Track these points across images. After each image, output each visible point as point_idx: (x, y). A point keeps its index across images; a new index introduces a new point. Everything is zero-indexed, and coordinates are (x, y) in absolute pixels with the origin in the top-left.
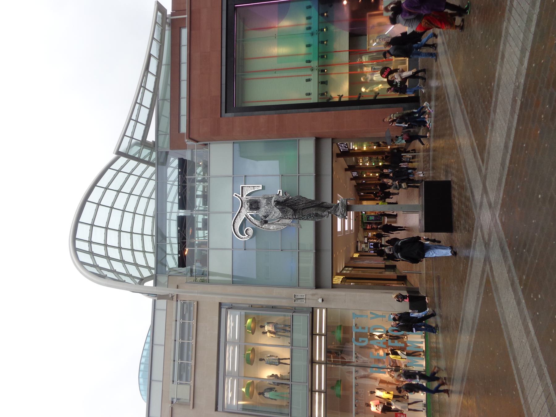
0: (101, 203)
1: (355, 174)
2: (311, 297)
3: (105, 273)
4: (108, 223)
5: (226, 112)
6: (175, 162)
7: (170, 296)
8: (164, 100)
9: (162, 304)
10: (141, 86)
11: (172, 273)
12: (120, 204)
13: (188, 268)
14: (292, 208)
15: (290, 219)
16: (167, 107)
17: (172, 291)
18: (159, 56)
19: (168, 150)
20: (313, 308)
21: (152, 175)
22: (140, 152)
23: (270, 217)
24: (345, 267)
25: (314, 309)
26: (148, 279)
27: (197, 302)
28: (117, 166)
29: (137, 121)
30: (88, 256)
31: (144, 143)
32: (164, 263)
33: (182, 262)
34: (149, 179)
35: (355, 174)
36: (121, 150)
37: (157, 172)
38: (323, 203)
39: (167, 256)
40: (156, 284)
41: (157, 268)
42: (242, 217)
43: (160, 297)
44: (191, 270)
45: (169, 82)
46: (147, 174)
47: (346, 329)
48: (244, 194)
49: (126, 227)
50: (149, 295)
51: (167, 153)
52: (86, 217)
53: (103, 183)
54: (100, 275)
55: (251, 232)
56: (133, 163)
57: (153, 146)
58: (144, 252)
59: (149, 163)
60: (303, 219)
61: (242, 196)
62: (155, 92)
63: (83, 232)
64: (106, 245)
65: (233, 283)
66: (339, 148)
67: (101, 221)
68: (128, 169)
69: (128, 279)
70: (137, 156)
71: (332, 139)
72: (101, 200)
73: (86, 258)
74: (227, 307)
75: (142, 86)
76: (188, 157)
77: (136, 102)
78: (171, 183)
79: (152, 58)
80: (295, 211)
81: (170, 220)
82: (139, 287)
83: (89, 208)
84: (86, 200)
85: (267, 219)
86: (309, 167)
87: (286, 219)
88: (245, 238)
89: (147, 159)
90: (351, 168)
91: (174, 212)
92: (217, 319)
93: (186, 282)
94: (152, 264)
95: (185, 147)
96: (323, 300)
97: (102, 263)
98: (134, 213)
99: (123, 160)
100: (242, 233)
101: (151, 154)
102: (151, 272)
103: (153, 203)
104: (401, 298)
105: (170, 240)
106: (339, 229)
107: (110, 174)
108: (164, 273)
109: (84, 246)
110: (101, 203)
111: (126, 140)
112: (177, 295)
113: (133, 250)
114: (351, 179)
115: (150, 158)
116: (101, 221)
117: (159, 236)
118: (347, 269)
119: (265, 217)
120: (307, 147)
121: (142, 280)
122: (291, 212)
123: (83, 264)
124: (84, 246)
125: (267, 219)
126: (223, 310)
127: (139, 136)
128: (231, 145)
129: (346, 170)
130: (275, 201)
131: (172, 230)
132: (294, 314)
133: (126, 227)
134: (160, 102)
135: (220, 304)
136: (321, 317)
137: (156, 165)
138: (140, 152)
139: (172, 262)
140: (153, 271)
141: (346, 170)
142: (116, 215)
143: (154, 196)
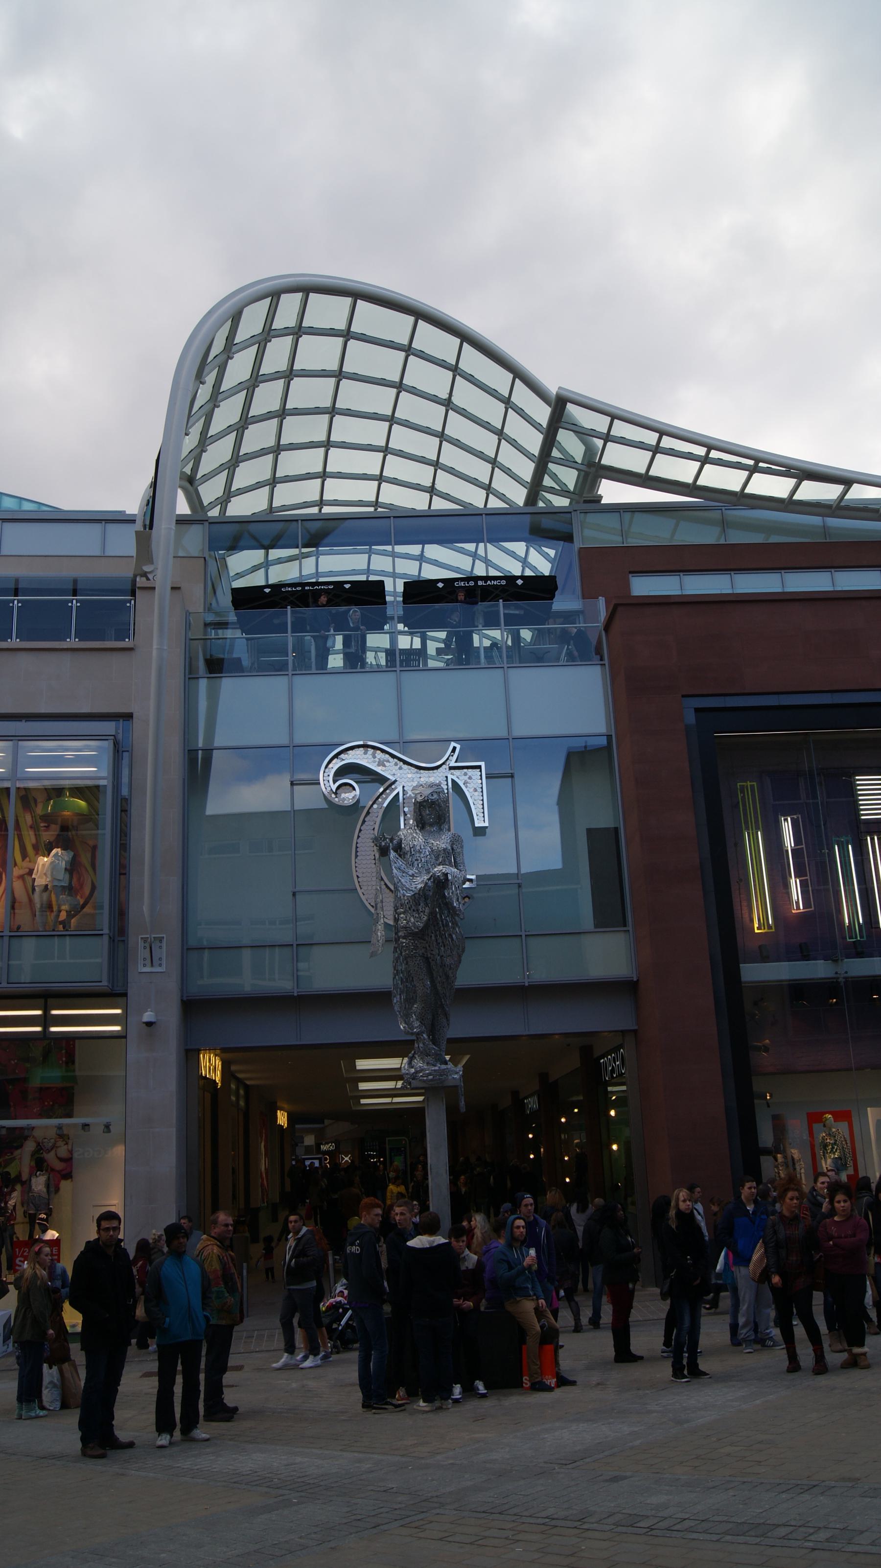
0: (411, 358)
1: (532, 1103)
2: (157, 983)
3: (210, 379)
4: (363, 338)
5: (697, 710)
6: (541, 561)
7: (146, 568)
8: (724, 524)
9: (124, 543)
10: (757, 460)
11: (212, 567)
12: (421, 374)
13: (232, 617)
14: (427, 926)
15: (396, 920)
16: (708, 536)
17: (163, 572)
18: (848, 508)
19: (578, 544)
20: (125, 995)
21: (501, 497)
22: (568, 461)
23: (400, 862)
24: (247, 1088)
25: (121, 1000)
26: (194, 499)
27: (131, 649)
28: (522, 396)
29: (656, 450)
30: (257, 329)
31: (593, 471)
32: (241, 543)
33: (247, 599)
34: (488, 488)
35: (532, 1103)
36: (570, 407)
37: (511, 512)
38: (446, 1015)
39: (262, 552)
40: (182, 521)
41: (224, 521)
42: (390, 770)
43: (144, 540)
44: (223, 625)
45: (775, 539)
46: (501, 482)
47: (61, 1100)
48: (457, 772)
49: (352, 395)
50: (151, 503)
51: (568, 538)
52: (370, 318)
53: (472, 361)
54: (204, 362)
55: (348, 797)
56: (534, 442)
57: (586, 496)
58: (273, 482)
59: (535, 489)
60: (397, 960)
61: (451, 768)
62: (741, 499)
63: (327, 311)
64: (290, 374)
65: (191, 755)
66: (609, 1053)
67: (359, 357)
68: (516, 427)
69: (190, 442)
70: (555, 453)
71: (635, 1031)
72: (422, 355)
73: (252, 323)
74: (120, 737)
75: (758, 463)
76: (560, 604)
77: (710, 448)
78: (481, 551)
79: (840, 488)
80: (419, 935)
81: (368, 571)
82: (169, 476)
83: (398, 326)
84: (419, 314)
85: (393, 854)
86: (546, 965)
87: (396, 909)
88: (326, 781)
89: (547, 481)
90: (550, 1092)
91: (396, 567)
92: (86, 708)
93: (188, 614)
94: (239, 508)
95: (588, 594)
96: (149, 1024)
97: (239, 368)
98: (392, 420)
99: (543, 413)
100: (341, 772)
101: (563, 492)
102: (212, 505)
103: (418, 502)
104: (143, 1345)
105: (307, 555)
106: (363, 1064)
107: (500, 379)
108: (214, 544)
109: (286, 317)
110: (411, 358)
111: (600, 423)
112: (154, 588)
113: (277, 449)
114: (515, 1094)
115: (551, 490)
116: (359, 357)
117: (319, 524)
118: (242, 1092)
119: (398, 848)
120: (608, 956)
121: (190, 482)
122: (415, 921)
123: (236, 318)
124: (286, 317)
125: (393, 854)
126: (109, 727)
127: (615, 456)
128: (603, 729)
129: (543, 1077)
130: (446, 875)
131: (339, 564)
132: (106, 939)
133: (352, 395)
134: (716, 515)
135: (129, 716)
136: (100, 1021)
137: (531, 509)
138: (568, 461)
139: (246, 567)
140: (214, 513)
141: (543, 1077)
142: (380, 400)
143: (439, 504)
